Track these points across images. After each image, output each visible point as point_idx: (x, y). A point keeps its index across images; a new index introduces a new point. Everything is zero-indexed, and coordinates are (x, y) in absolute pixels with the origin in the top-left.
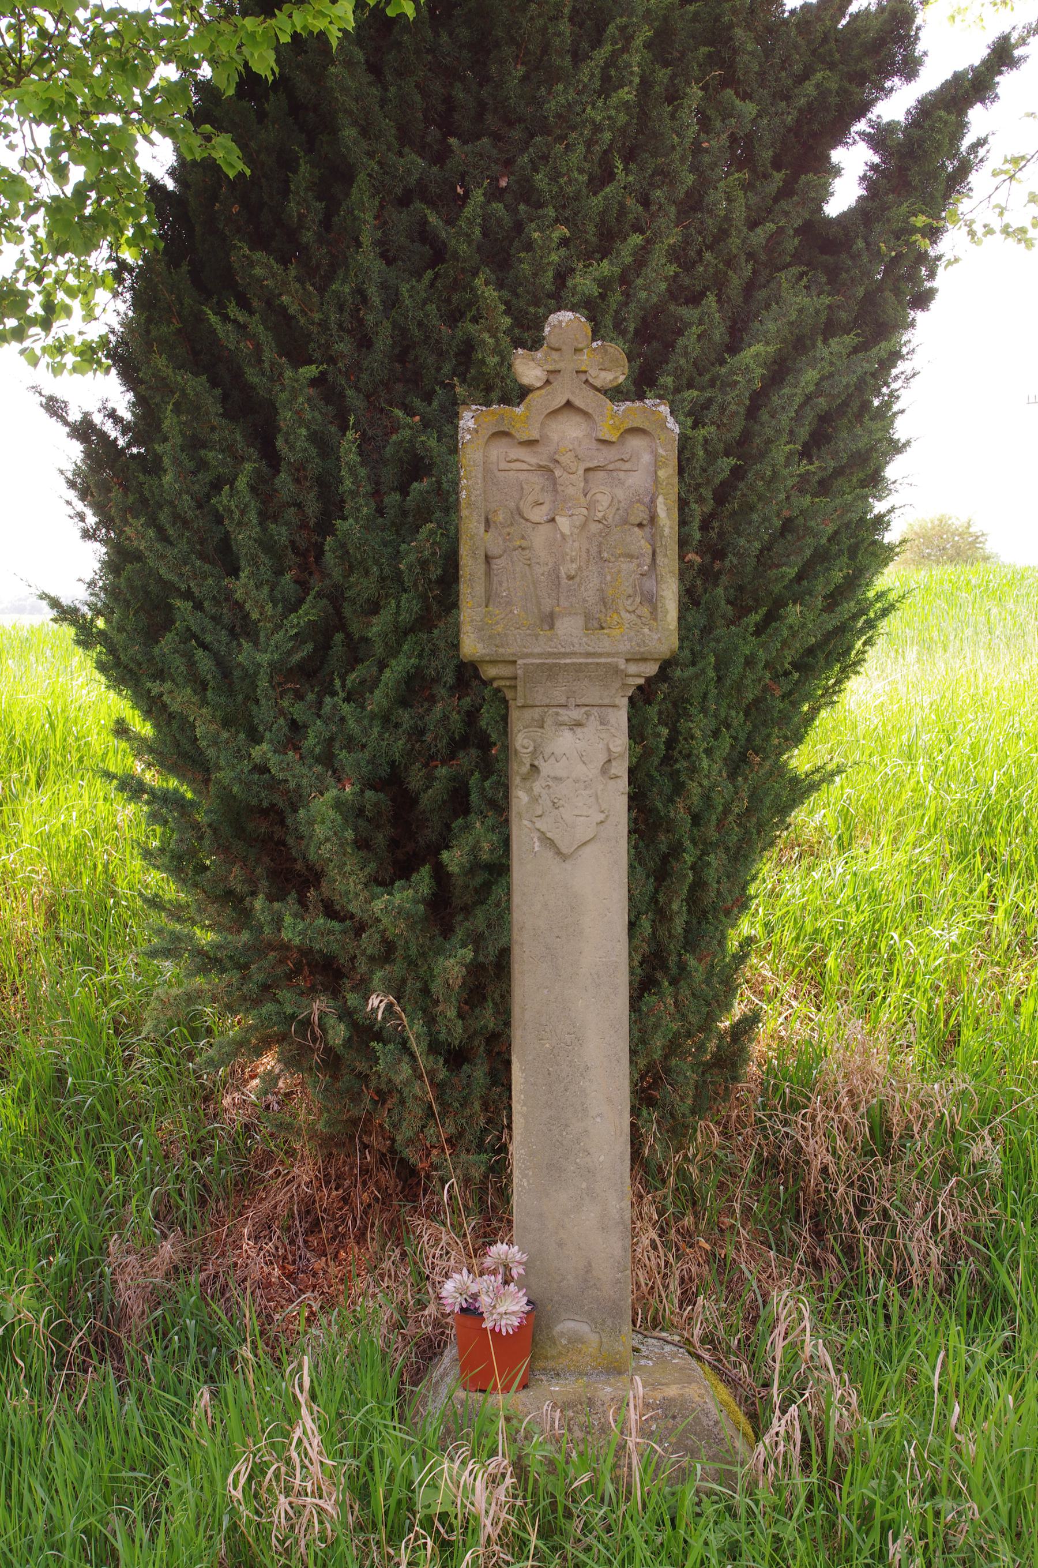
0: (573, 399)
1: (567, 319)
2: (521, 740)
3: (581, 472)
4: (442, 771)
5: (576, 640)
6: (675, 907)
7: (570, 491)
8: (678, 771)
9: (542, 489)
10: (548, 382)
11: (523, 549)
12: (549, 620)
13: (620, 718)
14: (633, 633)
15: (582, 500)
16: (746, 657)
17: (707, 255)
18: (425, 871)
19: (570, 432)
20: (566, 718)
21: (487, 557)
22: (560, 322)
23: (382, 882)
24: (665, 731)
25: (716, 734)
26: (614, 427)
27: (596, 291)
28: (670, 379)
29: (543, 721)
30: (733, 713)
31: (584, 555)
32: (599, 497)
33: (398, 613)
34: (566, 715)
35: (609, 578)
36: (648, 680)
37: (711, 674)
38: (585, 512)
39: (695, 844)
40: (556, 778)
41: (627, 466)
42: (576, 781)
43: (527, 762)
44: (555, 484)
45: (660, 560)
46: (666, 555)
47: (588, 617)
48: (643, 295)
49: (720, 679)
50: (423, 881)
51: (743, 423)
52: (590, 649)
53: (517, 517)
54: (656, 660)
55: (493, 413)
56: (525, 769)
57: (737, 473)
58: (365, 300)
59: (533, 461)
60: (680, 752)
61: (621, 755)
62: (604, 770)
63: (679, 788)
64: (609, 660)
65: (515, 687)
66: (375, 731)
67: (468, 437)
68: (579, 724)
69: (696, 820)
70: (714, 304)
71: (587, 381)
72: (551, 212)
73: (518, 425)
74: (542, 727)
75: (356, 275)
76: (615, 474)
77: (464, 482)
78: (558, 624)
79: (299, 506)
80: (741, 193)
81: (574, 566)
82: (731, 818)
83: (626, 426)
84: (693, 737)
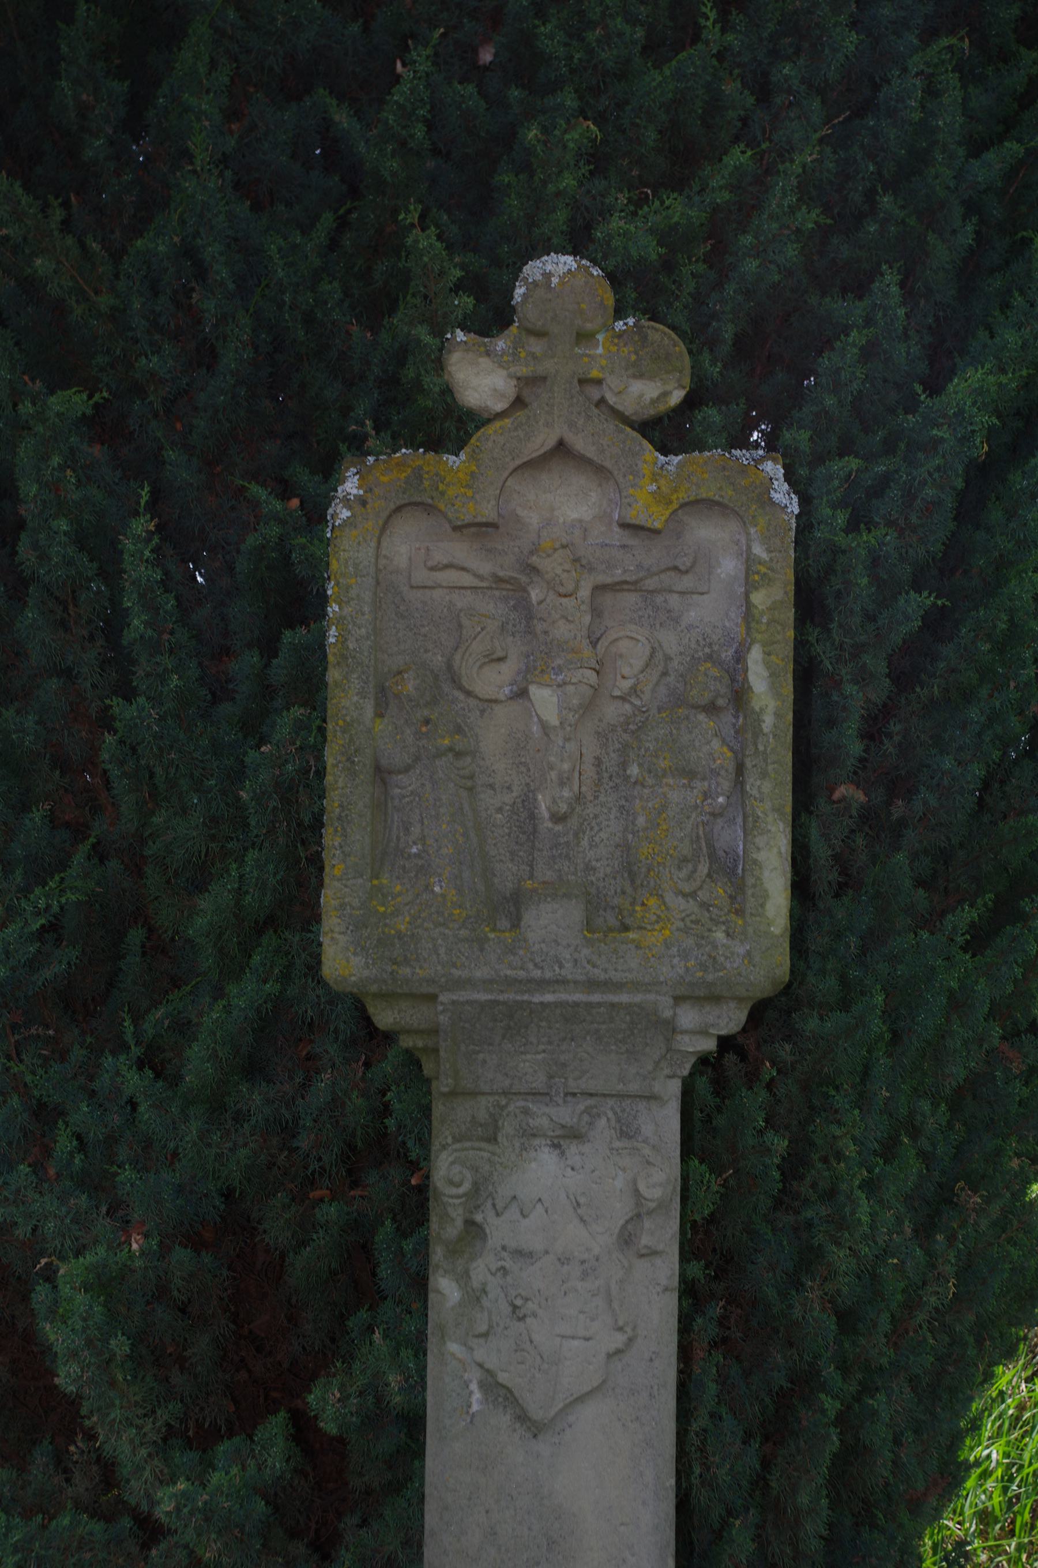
0: (571, 438)
1: (562, 269)
2: (448, 1169)
3: (585, 593)
4: (331, 1212)
5: (566, 955)
6: (804, 1499)
7: (562, 631)
8: (809, 1225)
9: (503, 628)
10: (519, 402)
11: (459, 755)
12: (511, 906)
13: (665, 1123)
14: (690, 942)
15: (587, 652)
16: (951, 994)
17: (886, 201)
18: (275, 1428)
19: (567, 507)
20: (545, 1122)
21: (378, 769)
22: (547, 276)
23: (194, 1438)
24: (780, 1144)
25: (889, 1150)
26: (659, 497)
27: (653, 252)
28: (804, 435)
29: (497, 1128)
30: (925, 1106)
31: (589, 771)
32: (624, 646)
33: (240, 893)
34: (546, 1116)
35: (641, 821)
36: (725, 1043)
37: (877, 1026)
38: (591, 677)
39: (844, 1368)
40: (519, 1253)
41: (687, 582)
42: (564, 1260)
43: (458, 1215)
44: (530, 617)
45: (753, 784)
46: (764, 775)
47: (594, 904)
48: (751, 266)
49: (896, 1037)
50: (273, 1447)
51: (952, 525)
52: (599, 974)
53: (446, 688)
54: (740, 1000)
55: (401, 465)
56: (453, 1230)
57: (937, 625)
58: (201, 272)
59: (485, 568)
60: (814, 1185)
61: (662, 1206)
62: (626, 1239)
63: (809, 1259)
64: (638, 998)
65: (436, 1050)
66: (194, 1127)
67: (345, 514)
68: (575, 1135)
69: (848, 1320)
70: (894, 289)
71: (602, 401)
72: (569, 100)
73: (451, 492)
74: (493, 1139)
75: (182, 222)
76: (659, 599)
77: (333, 609)
78: (529, 917)
79: (68, 674)
80: (953, 79)
81: (566, 793)
82: (921, 1317)
83: (682, 496)
84: (839, 1156)
